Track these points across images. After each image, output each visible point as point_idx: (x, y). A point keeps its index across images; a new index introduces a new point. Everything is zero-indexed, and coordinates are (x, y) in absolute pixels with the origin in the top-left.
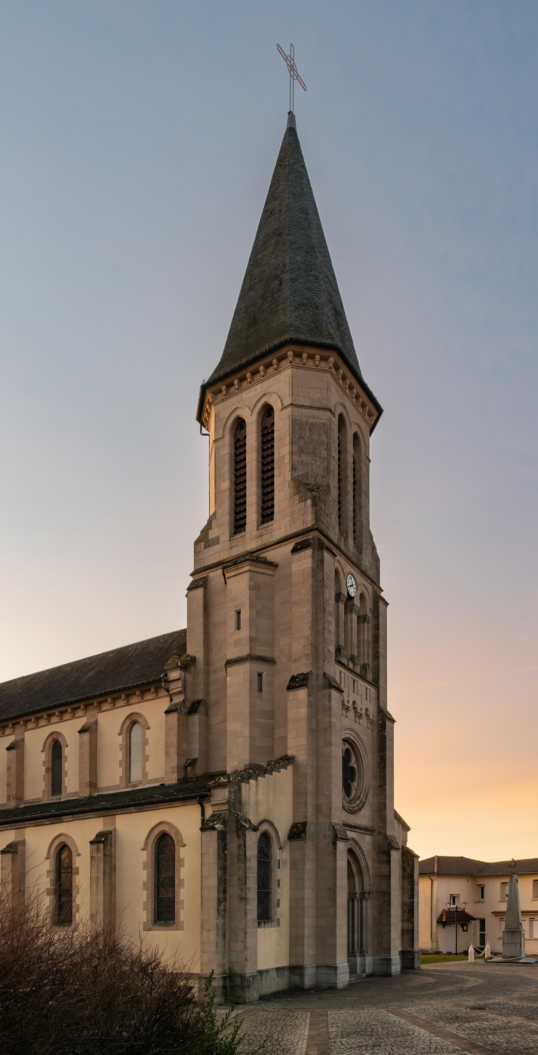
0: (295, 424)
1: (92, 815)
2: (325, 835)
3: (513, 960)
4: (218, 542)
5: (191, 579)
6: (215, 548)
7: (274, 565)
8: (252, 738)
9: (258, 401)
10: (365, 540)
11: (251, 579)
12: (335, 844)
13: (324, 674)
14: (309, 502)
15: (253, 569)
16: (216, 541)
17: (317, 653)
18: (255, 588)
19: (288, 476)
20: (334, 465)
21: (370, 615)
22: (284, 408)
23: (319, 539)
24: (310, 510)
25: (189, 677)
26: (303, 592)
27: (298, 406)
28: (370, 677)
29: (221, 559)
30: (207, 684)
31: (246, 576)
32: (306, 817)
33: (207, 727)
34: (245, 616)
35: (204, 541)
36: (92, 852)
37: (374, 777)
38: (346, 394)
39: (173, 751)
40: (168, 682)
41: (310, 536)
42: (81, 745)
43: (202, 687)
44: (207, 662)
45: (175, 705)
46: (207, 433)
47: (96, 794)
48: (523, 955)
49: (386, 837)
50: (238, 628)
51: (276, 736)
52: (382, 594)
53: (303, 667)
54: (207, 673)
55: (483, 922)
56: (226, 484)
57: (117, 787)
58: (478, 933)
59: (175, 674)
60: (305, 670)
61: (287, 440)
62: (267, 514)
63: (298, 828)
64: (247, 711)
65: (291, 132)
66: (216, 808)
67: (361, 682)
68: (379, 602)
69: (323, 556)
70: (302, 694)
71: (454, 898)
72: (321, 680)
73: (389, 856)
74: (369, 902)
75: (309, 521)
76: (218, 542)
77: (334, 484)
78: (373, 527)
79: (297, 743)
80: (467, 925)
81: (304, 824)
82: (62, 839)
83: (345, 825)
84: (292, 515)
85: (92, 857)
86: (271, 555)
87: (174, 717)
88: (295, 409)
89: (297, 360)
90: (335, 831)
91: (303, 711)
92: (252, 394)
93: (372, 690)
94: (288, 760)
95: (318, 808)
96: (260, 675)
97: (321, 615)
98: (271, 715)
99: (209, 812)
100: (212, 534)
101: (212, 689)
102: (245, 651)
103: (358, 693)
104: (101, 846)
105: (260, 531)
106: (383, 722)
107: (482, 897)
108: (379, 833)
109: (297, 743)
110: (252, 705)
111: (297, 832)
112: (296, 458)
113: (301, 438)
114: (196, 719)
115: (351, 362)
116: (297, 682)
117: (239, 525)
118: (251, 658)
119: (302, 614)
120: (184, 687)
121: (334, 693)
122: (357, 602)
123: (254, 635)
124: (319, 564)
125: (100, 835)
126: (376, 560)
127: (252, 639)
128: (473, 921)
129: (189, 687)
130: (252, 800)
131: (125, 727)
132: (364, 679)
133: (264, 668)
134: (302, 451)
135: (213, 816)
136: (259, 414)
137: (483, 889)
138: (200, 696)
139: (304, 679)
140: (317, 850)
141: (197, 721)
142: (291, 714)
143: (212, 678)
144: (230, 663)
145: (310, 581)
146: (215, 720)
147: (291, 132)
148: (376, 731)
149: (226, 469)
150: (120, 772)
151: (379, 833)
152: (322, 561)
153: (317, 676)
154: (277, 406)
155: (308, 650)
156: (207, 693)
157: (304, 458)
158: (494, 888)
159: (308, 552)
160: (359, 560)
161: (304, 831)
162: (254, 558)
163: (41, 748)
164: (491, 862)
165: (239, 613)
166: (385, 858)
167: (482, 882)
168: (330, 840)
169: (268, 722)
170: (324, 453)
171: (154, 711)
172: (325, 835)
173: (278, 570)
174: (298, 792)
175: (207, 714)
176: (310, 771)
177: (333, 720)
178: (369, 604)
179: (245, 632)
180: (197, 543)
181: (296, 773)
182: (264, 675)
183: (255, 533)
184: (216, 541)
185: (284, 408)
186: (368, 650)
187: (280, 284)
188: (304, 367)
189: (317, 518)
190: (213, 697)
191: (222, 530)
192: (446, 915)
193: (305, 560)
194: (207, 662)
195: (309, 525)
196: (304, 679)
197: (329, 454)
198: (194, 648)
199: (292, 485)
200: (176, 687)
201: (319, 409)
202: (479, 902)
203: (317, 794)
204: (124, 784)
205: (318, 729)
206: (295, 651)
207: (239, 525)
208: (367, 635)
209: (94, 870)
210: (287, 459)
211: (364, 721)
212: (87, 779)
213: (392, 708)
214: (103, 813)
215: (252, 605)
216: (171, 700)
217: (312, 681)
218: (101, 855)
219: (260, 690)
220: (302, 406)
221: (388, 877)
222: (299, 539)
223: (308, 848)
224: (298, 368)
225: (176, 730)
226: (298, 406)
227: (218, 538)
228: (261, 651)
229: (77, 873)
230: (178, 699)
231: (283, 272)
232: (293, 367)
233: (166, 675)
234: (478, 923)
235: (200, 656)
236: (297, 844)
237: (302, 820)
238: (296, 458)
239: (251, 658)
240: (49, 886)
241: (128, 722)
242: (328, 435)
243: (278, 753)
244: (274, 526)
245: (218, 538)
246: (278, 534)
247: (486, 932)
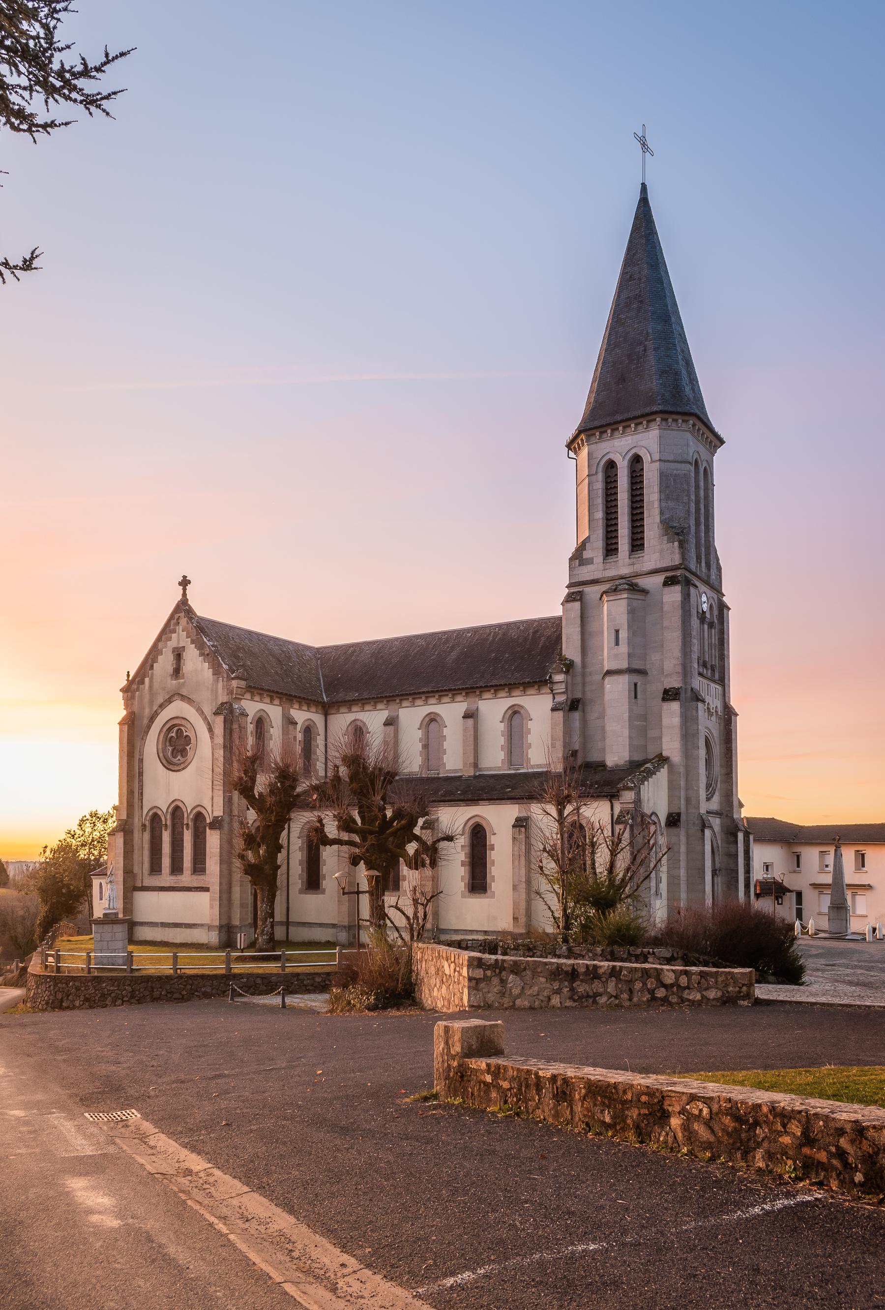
0: (663, 476)
1: (508, 801)
2: (694, 824)
3: (839, 936)
4: (592, 563)
5: (567, 591)
6: (590, 567)
7: (645, 592)
8: (630, 738)
9: (629, 451)
10: (712, 557)
11: (628, 605)
12: (703, 831)
13: (692, 689)
14: (676, 544)
15: (631, 596)
16: (590, 561)
17: (686, 672)
18: (631, 612)
19: (658, 519)
20: (693, 510)
21: (716, 621)
22: (652, 461)
23: (686, 577)
24: (677, 551)
25: (569, 677)
26: (674, 620)
27: (665, 461)
28: (717, 676)
29: (596, 577)
30: (584, 684)
31: (625, 602)
32: (680, 808)
33: (584, 722)
34: (623, 635)
35: (578, 558)
36: (514, 833)
37: (721, 766)
38: (698, 441)
39: (559, 744)
40: (552, 683)
41: (678, 573)
42: (465, 730)
43: (580, 687)
44: (584, 665)
45: (559, 703)
46: (574, 456)
47: (477, 774)
48: (849, 931)
49: (733, 820)
50: (617, 644)
51: (649, 736)
52: (724, 599)
53: (675, 682)
54: (584, 675)
55: (799, 895)
56: (600, 515)
57: (499, 768)
58: (795, 907)
59: (559, 677)
60: (677, 685)
61: (656, 489)
62: (637, 544)
63: (674, 817)
64: (626, 715)
65: (644, 202)
66: (625, 806)
67: (713, 685)
68: (722, 608)
69: (689, 591)
70: (675, 707)
71: (767, 867)
72: (689, 694)
73: (736, 837)
74: (719, 879)
75: (677, 560)
76: (592, 563)
77: (692, 522)
78: (717, 544)
79: (671, 746)
80: (781, 898)
81: (679, 814)
82: (477, 819)
83: (708, 812)
84: (661, 551)
85: (514, 839)
86: (643, 582)
87: (560, 715)
88: (662, 463)
89: (664, 423)
90: (703, 820)
91: (676, 720)
92: (622, 443)
93: (719, 688)
94: (662, 760)
95: (688, 800)
96: (636, 685)
97: (688, 639)
98: (644, 717)
99: (617, 809)
100: (587, 554)
101: (587, 689)
102: (624, 665)
103: (710, 692)
104: (523, 829)
105: (632, 560)
106: (728, 716)
107: (798, 866)
108: (727, 816)
109: (671, 746)
110: (630, 711)
111: (673, 820)
112: (664, 504)
113: (667, 487)
114: (577, 715)
115: (705, 420)
116: (670, 695)
117: (610, 549)
118: (630, 671)
119: (673, 638)
120: (566, 688)
121: (700, 705)
122: (708, 615)
123: (631, 651)
124: (686, 597)
125: (518, 820)
126: (719, 569)
127: (630, 655)
128: (788, 894)
129: (570, 688)
130: (646, 798)
131: (507, 716)
132: (714, 681)
133: (636, 678)
134: (668, 498)
135: (621, 812)
136: (629, 461)
137: (798, 857)
138: (579, 695)
139: (677, 694)
140: (688, 836)
141: (577, 718)
142: (665, 721)
143: (588, 679)
144: (609, 673)
145: (680, 612)
146: (592, 715)
147: (644, 202)
148: (722, 724)
149: (600, 501)
150: (502, 755)
151: (727, 816)
152: (689, 595)
153: (686, 689)
154: (646, 458)
155: (679, 669)
156: (584, 692)
157: (671, 504)
158: (811, 855)
159: (677, 588)
160: (709, 576)
161: (679, 820)
162: (631, 586)
163: (418, 726)
164: (806, 825)
165: (617, 631)
166: (732, 839)
167: (798, 849)
168: (699, 828)
169: (643, 724)
170: (685, 499)
171: (538, 707)
172: (694, 824)
173: (648, 596)
174: (672, 787)
175: (584, 711)
176: (682, 770)
177: (700, 727)
178: (716, 612)
179: (623, 648)
180: (571, 559)
181: (671, 771)
182: (638, 685)
183: (627, 560)
184: (590, 561)
185: (652, 461)
186: (715, 652)
187: (645, 350)
188: (669, 428)
189: (683, 557)
190: (589, 695)
191: (595, 552)
192: (760, 886)
193: (674, 595)
194: (584, 665)
195: (677, 563)
196: (677, 694)
197: (689, 499)
198: (570, 649)
199: (661, 527)
200: (561, 688)
201: (681, 462)
202: (795, 872)
203: (688, 788)
204: (506, 767)
205: (688, 735)
206: (668, 666)
207: (610, 549)
208: (715, 640)
209: (516, 849)
210: (656, 504)
211: (714, 718)
212: (472, 760)
213: (733, 703)
214: (519, 801)
215: (629, 627)
216: (554, 698)
217: (683, 695)
218: (523, 836)
219: (636, 697)
220: (668, 461)
221: (736, 856)
222: (669, 574)
223: (682, 835)
224: (664, 429)
225: (562, 725)
226: (665, 461)
227: (592, 559)
228: (637, 665)
229: (493, 849)
230: (561, 698)
231: (646, 340)
232: (660, 429)
233: (550, 677)
234: (794, 895)
235: (577, 660)
236: (674, 830)
237: (677, 811)
238: (664, 504)
239: (630, 671)
240: (463, 859)
241: (510, 712)
242: (688, 484)
243: (652, 752)
244: (645, 558)
245: (592, 559)
246: (649, 566)
247: (803, 907)
